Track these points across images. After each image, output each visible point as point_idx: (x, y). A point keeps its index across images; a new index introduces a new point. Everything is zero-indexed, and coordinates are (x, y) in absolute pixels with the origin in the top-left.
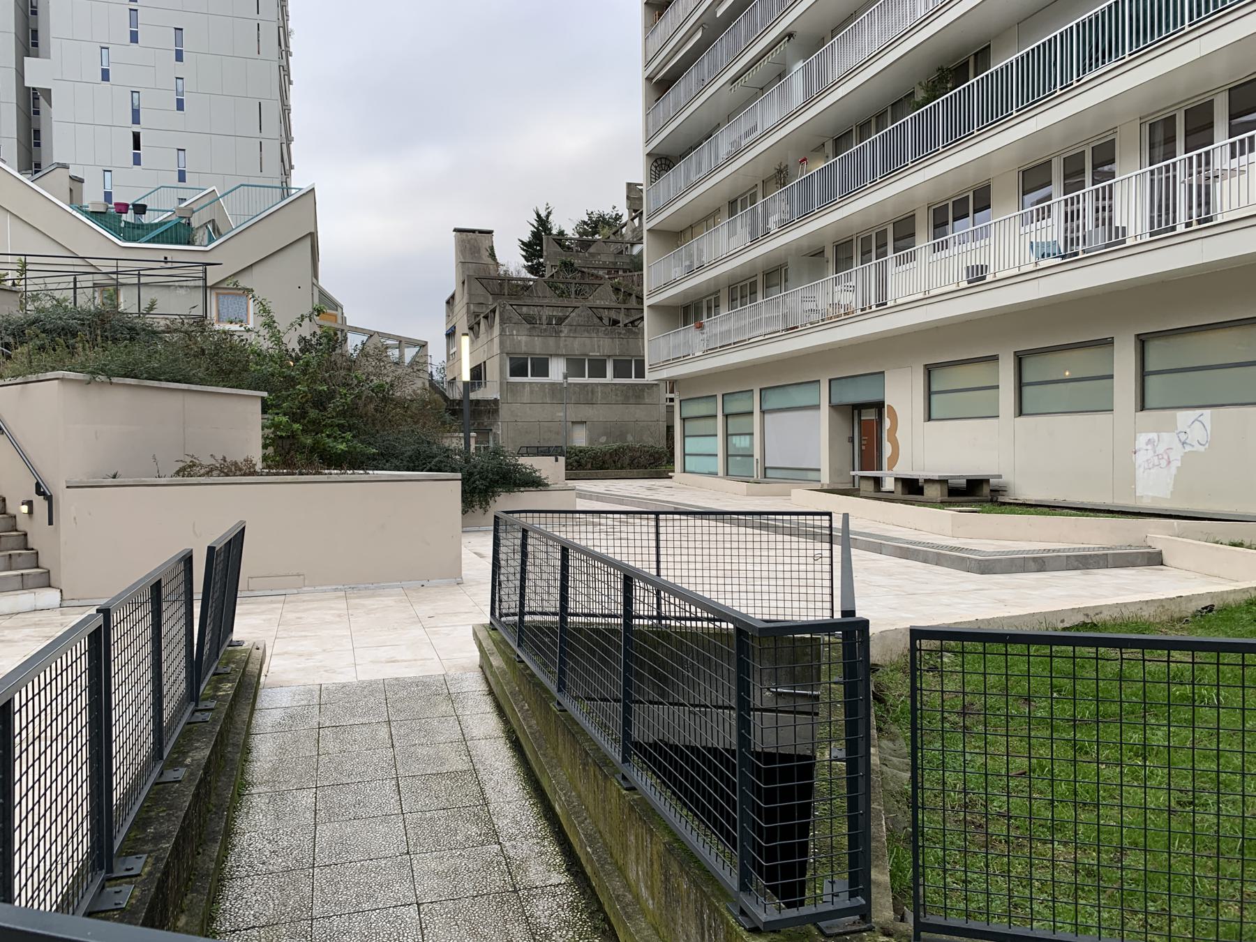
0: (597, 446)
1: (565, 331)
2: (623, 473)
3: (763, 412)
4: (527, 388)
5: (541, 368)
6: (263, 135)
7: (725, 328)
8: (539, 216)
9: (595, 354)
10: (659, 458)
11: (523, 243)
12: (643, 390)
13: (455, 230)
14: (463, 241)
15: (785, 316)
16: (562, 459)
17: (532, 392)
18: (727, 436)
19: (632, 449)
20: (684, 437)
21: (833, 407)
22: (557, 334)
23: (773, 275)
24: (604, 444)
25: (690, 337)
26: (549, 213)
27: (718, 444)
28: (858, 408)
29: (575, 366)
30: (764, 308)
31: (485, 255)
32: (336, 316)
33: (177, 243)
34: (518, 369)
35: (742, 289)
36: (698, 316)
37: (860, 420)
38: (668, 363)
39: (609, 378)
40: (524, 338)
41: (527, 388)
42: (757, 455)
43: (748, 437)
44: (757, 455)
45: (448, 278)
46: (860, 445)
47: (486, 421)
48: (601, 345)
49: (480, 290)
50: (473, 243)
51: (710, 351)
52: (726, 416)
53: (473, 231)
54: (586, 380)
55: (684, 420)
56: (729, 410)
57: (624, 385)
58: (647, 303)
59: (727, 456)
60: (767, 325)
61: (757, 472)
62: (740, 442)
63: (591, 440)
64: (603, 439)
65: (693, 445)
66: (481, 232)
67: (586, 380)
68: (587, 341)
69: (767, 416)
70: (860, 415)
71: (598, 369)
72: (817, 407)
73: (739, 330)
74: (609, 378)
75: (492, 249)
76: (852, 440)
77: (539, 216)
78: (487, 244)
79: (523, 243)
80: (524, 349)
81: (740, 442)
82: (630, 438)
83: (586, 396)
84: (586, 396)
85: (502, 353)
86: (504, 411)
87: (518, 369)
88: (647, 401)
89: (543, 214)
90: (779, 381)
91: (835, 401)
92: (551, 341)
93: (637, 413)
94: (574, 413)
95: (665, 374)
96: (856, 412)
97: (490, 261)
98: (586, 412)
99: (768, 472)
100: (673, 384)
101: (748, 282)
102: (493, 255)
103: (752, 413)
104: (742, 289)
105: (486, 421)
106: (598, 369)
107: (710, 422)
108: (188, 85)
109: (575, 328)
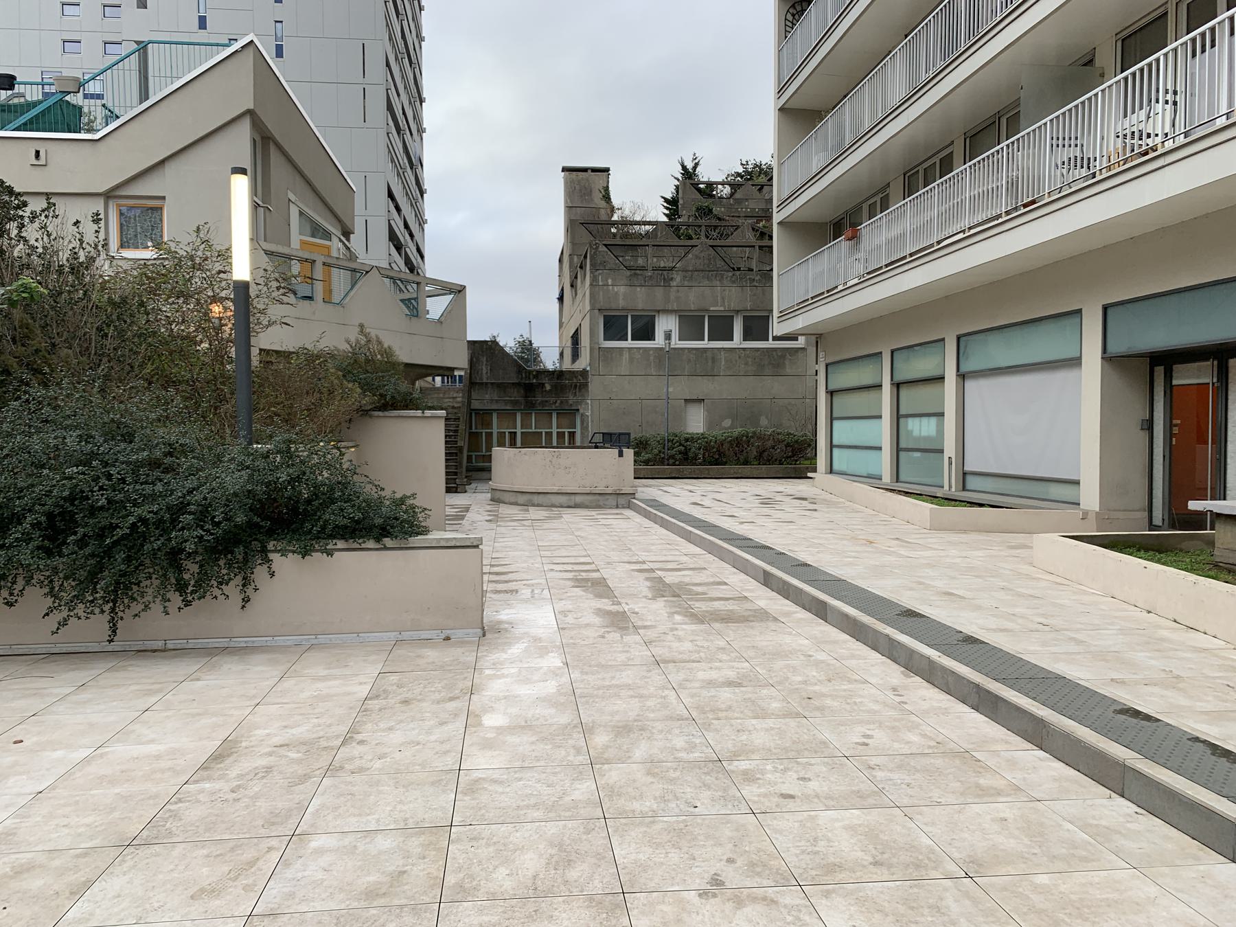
0: (717, 432)
1: (678, 278)
2: (747, 469)
3: (962, 376)
4: (626, 355)
5: (646, 332)
6: (367, 80)
7: (896, 231)
8: (684, 167)
9: (718, 308)
10: (801, 450)
11: (666, 200)
12: (783, 357)
13: (564, 169)
14: (572, 181)
15: (1013, 185)
16: (629, 453)
17: (631, 360)
18: (898, 417)
19: (760, 437)
20: (832, 419)
21: (1108, 358)
22: (667, 282)
23: (989, 126)
24: (728, 428)
25: (836, 259)
26: (697, 165)
27: (882, 431)
28: (1165, 360)
29: (691, 325)
30: (973, 183)
31: (598, 201)
32: (328, 248)
33: (70, 132)
34: (614, 327)
35: (923, 168)
36: (855, 225)
37: (1169, 388)
38: (805, 305)
39: (737, 341)
40: (622, 289)
41: (626, 355)
42: (950, 449)
43: (933, 420)
44: (950, 449)
45: (550, 230)
46: (1169, 435)
47: (571, 399)
48: (725, 296)
49: (585, 237)
50: (586, 186)
51: (874, 274)
52: (897, 386)
53: (585, 170)
54: (705, 344)
55: (831, 393)
56: (904, 374)
57: (758, 349)
58: (777, 218)
59: (898, 450)
60: (973, 211)
61: (949, 484)
62: (920, 429)
63: (710, 423)
64: (727, 423)
65: (845, 432)
66: (594, 170)
67: (705, 344)
68: (707, 291)
69: (970, 385)
70: (1169, 376)
71: (722, 329)
72: (1075, 362)
73: (918, 231)
74: (737, 341)
75: (607, 189)
76: (1149, 425)
77: (684, 167)
78: (602, 184)
79: (666, 200)
80: (622, 303)
81: (920, 429)
82: (764, 421)
83: (705, 364)
84: (705, 364)
85: (592, 309)
86: (594, 386)
87: (614, 327)
88: (788, 371)
89: (690, 166)
90: (1003, 317)
91: (1115, 348)
92: (659, 292)
93: (772, 387)
94: (680, 388)
95: (799, 323)
96: (1160, 371)
97: (603, 204)
98: (704, 386)
99: (969, 479)
100: (819, 338)
101: (937, 159)
102: (607, 197)
103: (941, 379)
104: (923, 168)
105: (571, 399)
106: (722, 329)
107: (872, 395)
108: (287, 29)
109: (689, 274)
